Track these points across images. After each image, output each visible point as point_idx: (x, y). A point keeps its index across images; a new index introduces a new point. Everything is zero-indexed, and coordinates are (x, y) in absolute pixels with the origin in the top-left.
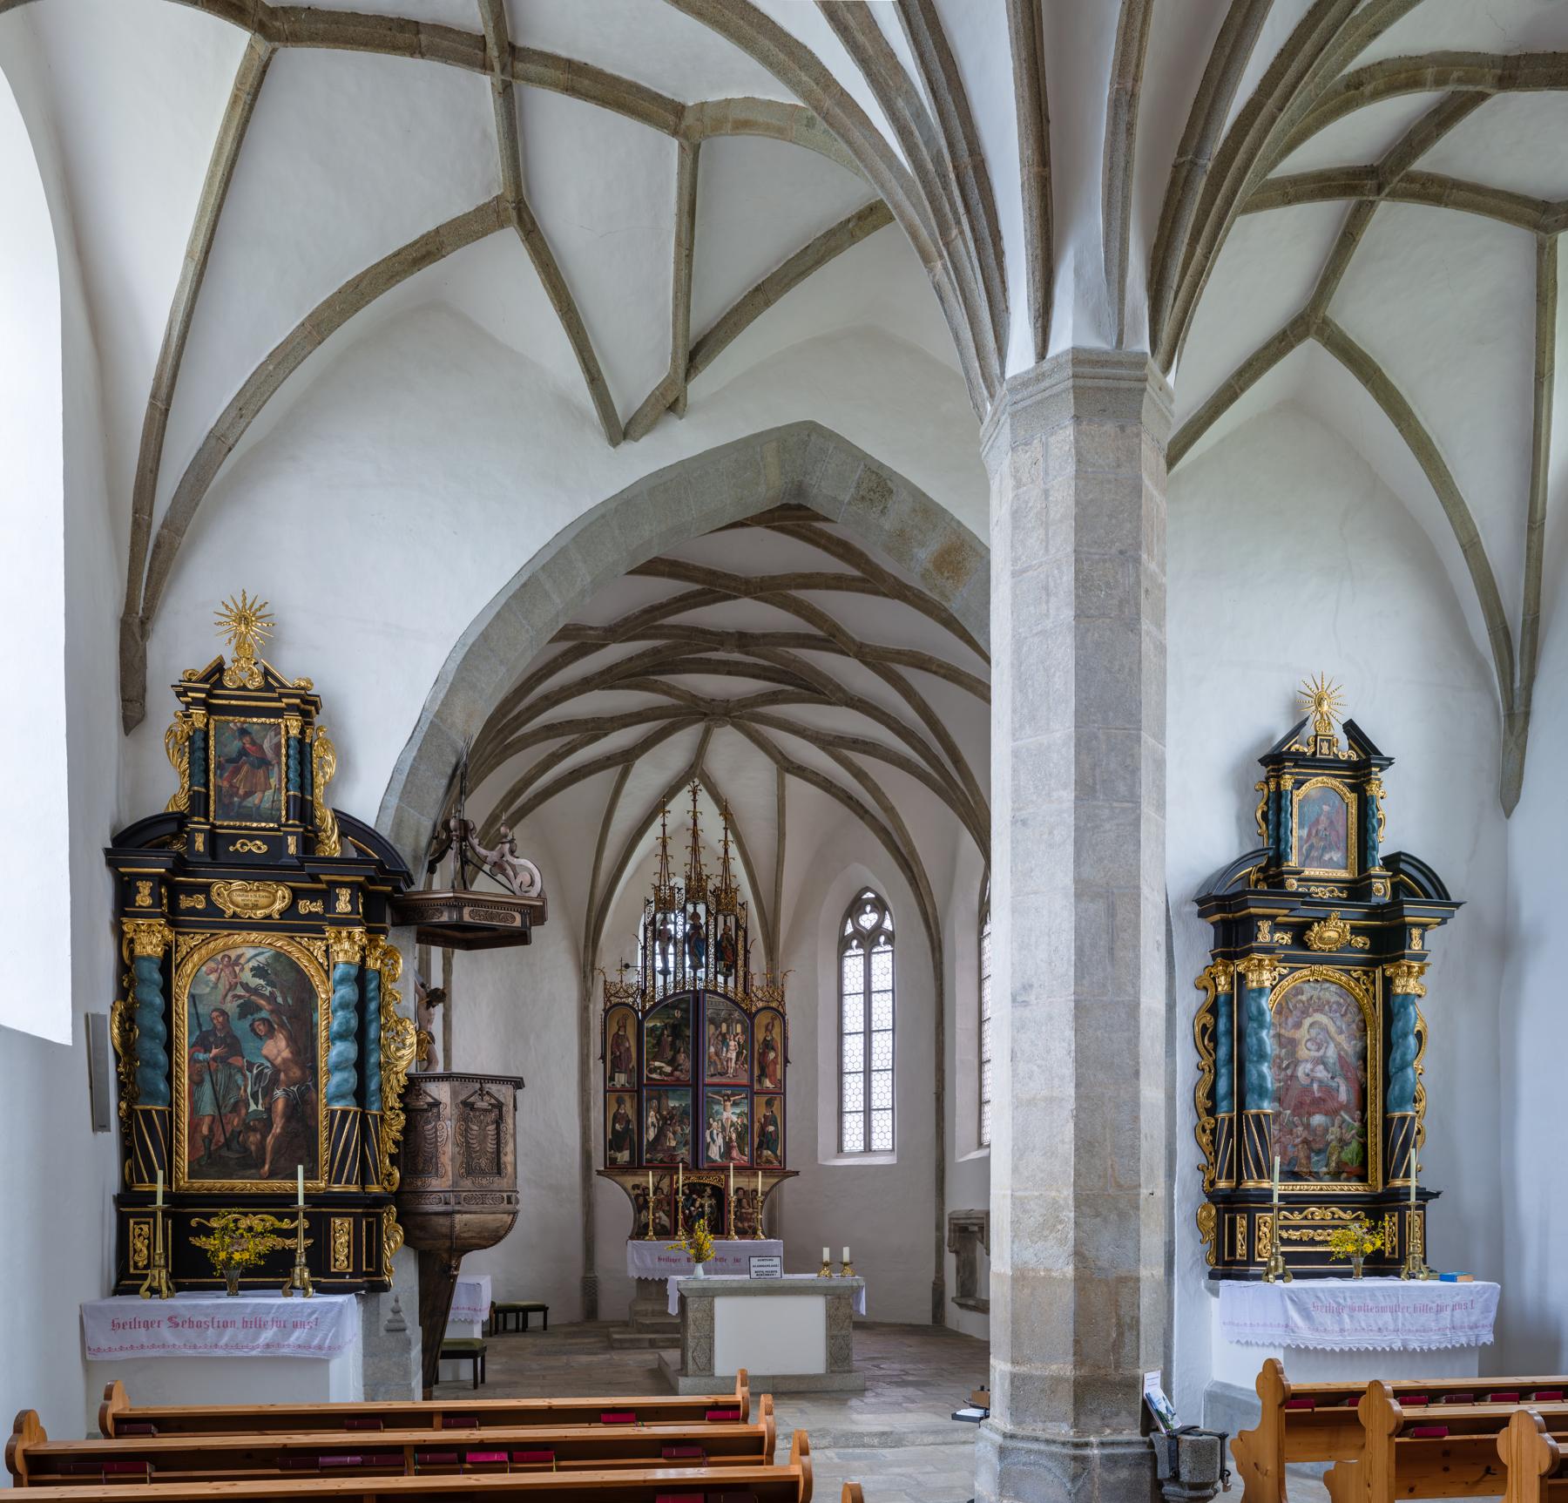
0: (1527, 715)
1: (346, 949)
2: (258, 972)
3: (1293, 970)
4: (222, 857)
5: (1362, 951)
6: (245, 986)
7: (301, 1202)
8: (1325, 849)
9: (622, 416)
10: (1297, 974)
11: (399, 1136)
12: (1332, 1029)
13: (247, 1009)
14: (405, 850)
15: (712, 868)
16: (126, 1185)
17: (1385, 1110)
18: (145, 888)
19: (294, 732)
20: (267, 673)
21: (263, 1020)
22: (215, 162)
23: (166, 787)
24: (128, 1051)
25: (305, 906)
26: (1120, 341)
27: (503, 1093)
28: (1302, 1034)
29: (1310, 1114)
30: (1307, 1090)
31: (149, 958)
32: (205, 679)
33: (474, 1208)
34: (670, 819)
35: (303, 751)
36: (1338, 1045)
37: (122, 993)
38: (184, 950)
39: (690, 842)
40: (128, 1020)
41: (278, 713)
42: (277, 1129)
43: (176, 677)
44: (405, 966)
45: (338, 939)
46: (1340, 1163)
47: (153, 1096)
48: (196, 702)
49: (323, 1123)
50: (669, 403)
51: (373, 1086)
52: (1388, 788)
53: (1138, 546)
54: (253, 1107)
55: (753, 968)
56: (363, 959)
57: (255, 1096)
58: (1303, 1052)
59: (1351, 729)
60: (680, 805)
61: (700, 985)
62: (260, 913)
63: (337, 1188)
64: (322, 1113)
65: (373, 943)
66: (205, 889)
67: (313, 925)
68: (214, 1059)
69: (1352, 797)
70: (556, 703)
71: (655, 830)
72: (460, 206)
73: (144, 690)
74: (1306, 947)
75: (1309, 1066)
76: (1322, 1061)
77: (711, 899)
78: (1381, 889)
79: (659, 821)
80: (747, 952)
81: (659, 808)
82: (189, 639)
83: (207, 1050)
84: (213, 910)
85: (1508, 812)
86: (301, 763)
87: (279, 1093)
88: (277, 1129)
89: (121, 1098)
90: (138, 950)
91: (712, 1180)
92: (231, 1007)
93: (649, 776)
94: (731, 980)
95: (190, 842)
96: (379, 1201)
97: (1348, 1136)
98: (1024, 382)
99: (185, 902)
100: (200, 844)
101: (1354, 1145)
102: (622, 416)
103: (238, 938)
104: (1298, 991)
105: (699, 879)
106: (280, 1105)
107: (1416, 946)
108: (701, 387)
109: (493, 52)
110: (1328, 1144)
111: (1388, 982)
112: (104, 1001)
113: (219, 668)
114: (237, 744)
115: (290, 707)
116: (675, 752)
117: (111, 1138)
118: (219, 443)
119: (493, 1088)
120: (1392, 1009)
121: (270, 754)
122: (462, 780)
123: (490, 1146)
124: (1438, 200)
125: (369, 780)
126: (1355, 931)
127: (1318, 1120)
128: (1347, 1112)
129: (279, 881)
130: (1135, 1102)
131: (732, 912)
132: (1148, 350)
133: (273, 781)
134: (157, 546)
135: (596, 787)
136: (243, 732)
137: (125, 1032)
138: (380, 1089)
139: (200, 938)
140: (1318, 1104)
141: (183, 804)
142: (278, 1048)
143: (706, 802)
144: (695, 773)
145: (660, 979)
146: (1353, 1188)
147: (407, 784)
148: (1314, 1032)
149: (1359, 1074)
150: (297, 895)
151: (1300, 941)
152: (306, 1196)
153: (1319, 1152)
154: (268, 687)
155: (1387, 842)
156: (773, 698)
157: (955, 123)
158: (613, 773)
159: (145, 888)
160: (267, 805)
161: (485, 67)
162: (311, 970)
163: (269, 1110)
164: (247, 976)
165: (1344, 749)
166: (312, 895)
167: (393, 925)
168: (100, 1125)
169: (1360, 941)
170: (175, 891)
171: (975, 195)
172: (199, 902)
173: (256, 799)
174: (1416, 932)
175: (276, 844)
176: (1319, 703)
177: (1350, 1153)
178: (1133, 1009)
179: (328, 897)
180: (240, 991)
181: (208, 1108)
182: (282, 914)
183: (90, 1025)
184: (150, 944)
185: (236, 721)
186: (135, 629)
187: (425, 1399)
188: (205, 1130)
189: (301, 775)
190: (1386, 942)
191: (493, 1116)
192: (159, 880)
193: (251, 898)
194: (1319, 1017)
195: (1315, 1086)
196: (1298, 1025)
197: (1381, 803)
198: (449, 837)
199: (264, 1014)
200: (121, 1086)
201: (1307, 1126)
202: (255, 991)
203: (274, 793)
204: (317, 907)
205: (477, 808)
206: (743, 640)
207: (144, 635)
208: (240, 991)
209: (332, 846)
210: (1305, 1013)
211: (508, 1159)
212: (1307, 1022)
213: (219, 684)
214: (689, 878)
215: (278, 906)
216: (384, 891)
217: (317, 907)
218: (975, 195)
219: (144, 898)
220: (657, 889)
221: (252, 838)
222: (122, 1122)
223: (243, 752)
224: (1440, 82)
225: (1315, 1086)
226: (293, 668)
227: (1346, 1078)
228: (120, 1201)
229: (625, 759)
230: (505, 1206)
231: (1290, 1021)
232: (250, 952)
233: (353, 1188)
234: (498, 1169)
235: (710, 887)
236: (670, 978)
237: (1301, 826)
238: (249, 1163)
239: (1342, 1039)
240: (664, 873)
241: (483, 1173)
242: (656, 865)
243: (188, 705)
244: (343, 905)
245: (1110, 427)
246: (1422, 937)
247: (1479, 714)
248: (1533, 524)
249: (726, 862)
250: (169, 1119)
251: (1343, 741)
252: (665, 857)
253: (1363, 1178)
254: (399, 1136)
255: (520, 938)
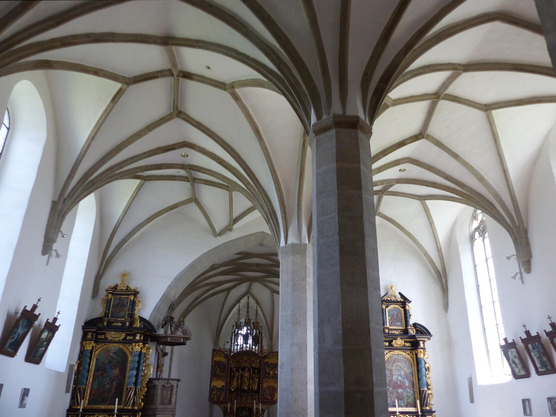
0: (447, 289)
1: (137, 348)
2: (114, 353)
3: (390, 352)
4: (110, 327)
5: (409, 347)
6: (111, 357)
7: (116, 411)
8: (396, 322)
9: (218, 230)
10: (391, 353)
11: (144, 394)
12: (402, 367)
13: (110, 362)
14: (155, 325)
15: (252, 317)
16: (71, 406)
17: (419, 388)
18: (90, 334)
19: (132, 299)
20: (127, 286)
21: (114, 365)
22: (131, 197)
23: (99, 311)
24: (78, 373)
25: (129, 338)
26: (301, 242)
27: (174, 383)
28: (394, 368)
29: (398, 389)
30: (396, 383)
31: (88, 350)
32: (112, 288)
33: (162, 413)
34: (241, 304)
35: (133, 303)
36: (404, 371)
37: (80, 358)
38: (97, 348)
39: (246, 310)
40: (79, 365)
41: (129, 295)
42: (112, 392)
43: (107, 288)
44: (152, 351)
45: (135, 346)
46: (407, 402)
47: (82, 384)
48: (110, 293)
49: (125, 390)
50: (228, 228)
51: (139, 381)
52: (411, 307)
53: (306, 277)
54: (107, 386)
55: (263, 344)
56: (141, 350)
57: (108, 384)
58: (394, 373)
59: (400, 293)
60: (244, 300)
61: (248, 349)
62: (117, 339)
63: (126, 408)
64: (125, 388)
65: (144, 346)
66: (105, 334)
67: (130, 342)
68: (100, 374)
69: (402, 309)
70: (207, 279)
71: (237, 307)
72: (183, 199)
73: (98, 290)
74: (392, 346)
75: (396, 376)
76: (400, 375)
77: (252, 325)
78: (412, 332)
79: (238, 305)
80: (262, 339)
81: (238, 301)
82: (111, 279)
83: (98, 372)
84: (106, 338)
85: (447, 312)
86: (133, 306)
87: (115, 383)
88: (112, 392)
89: (74, 384)
90: (86, 348)
91: (248, 406)
92: (106, 362)
93: (235, 293)
94: (257, 347)
95: (103, 323)
96: (137, 411)
97: (409, 395)
98: (283, 247)
99: (99, 337)
100: (105, 324)
101: (412, 398)
102: (218, 230)
103: (111, 345)
104: (391, 357)
105: (248, 319)
106: (114, 386)
107: (422, 345)
108: (235, 226)
109: (190, 179)
110: (404, 397)
111: (416, 355)
112: (75, 362)
113: (117, 286)
114: (118, 302)
115: (132, 294)
116: (243, 288)
117: (69, 395)
118: (124, 241)
119: (171, 382)
120: (418, 362)
121: (125, 303)
122: (172, 307)
123: (169, 397)
124: (396, 195)
125: (148, 309)
126: (405, 342)
127: (400, 391)
128: (409, 388)
129: (123, 332)
130: (306, 389)
131: (258, 329)
132: (307, 242)
133: (125, 310)
134: (107, 261)
135: (221, 296)
136: (120, 299)
137: (78, 367)
138: (141, 382)
139: (101, 345)
140: (400, 387)
141: (103, 314)
142: (116, 372)
143: (251, 299)
144: (248, 293)
145: (236, 347)
146: (412, 409)
147: (157, 309)
148: (397, 367)
149: (411, 378)
150: (127, 335)
151: (390, 344)
152: (118, 410)
153: (401, 400)
154: (127, 289)
155: (412, 321)
156: (268, 277)
157: (269, 207)
158: (226, 293)
159: (90, 334)
160: (123, 315)
161: (188, 181)
162: (128, 353)
163: (111, 387)
164: (112, 354)
165: (399, 298)
166: (131, 335)
167: (151, 341)
168: (67, 391)
169: (408, 344)
170: (97, 334)
171: (273, 217)
172: (103, 337)
173: (120, 313)
174: (421, 342)
175: (124, 323)
176: (392, 288)
177: (411, 400)
178: (306, 369)
179: (135, 336)
180: (109, 358)
181: (96, 387)
182: (123, 339)
183: (71, 367)
184: (89, 348)
185: (118, 297)
186: (99, 277)
187: (35, 356)
188: (94, 392)
189: (132, 308)
190: (415, 345)
191: (170, 389)
192: (93, 332)
193: (115, 336)
194: (398, 363)
195: (399, 382)
196: (392, 366)
197: (410, 311)
198: (168, 321)
199: (114, 363)
200: (75, 381)
201: (397, 392)
202: (113, 358)
203: (126, 312)
204: (131, 338)
205: (176, 315)
206: (257, 265)
207: (101, 278)
208: (109, 358)
209: (138, 324)
210: (394, 362)
211: (173, 400)
212: (395, 365)
213: (116, 289)
214: (246, 320)
215: (122, 338)
216: (148, 333)
217: (131, 338)
218: (273, 217)
219: (89, 336)
220: (236, 323)
221: (118, 322)
222: (73, 390)
223: (119, 303)
224: (381, 184)
225: (399, 382)
226: (132, 287)
227: (408, 379)
228: (68, 411)
229: (229, 290)
230: (171, 412)
231: (390, 365)
232: (113, 348)
233: (130, 408)
234: (170, 403)
235: (252, 322)
236: (239, 347)
237: (389, 316)
238: (103, 402)
239: (405, 369)
240: (239, 318)
241: (166, 404)
242: (236, 316)
243: (108, 293)
244: (138, 338)
245: (300, 256)
246: (424, 343)
247: (436, 289)
248: (439, 250)
249: (257, 314)
250: (84, 390)
251: (399, 296)
252: (239, 314)
253: (415, 406)
254: (144, 394)
255: (183, 344)
